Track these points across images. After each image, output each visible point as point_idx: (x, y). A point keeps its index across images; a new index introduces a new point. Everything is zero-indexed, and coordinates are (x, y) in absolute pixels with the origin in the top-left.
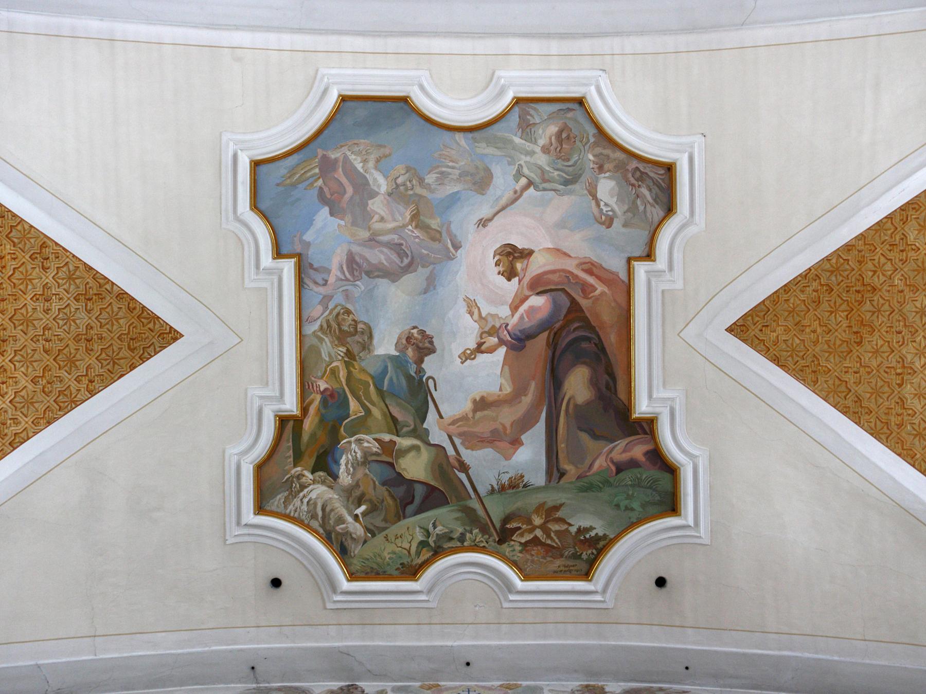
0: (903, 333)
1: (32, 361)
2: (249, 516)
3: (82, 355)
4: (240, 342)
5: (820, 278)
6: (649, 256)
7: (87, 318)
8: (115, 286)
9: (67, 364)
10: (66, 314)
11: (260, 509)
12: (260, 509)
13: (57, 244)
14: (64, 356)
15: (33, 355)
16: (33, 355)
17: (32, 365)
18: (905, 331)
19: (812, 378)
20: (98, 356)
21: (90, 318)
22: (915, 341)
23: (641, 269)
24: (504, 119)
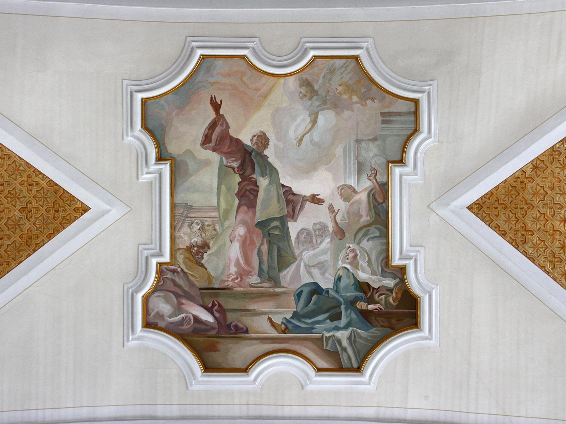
0: (499, 209)
1: (20, 225)
2: (423, 98)
3: (501, 197)
4: (429, 205)
5: (526, 173)
6: (401, 161)
7: (55, 197)
8: (45, 176)
9: (44, 227)
10: (41, 194)
11: (416, 102)
12: (416, 102)
13: (9, 150)
14: (12, 222)
15: (47, 220)
16: (47, 220)
17: (19, 227)
18: (525, 207)
19: (530, 235)
20: (61, 222)
21: (56, 197)
22: (561, 213)
23: (397, 171)
24: (360, 416)
